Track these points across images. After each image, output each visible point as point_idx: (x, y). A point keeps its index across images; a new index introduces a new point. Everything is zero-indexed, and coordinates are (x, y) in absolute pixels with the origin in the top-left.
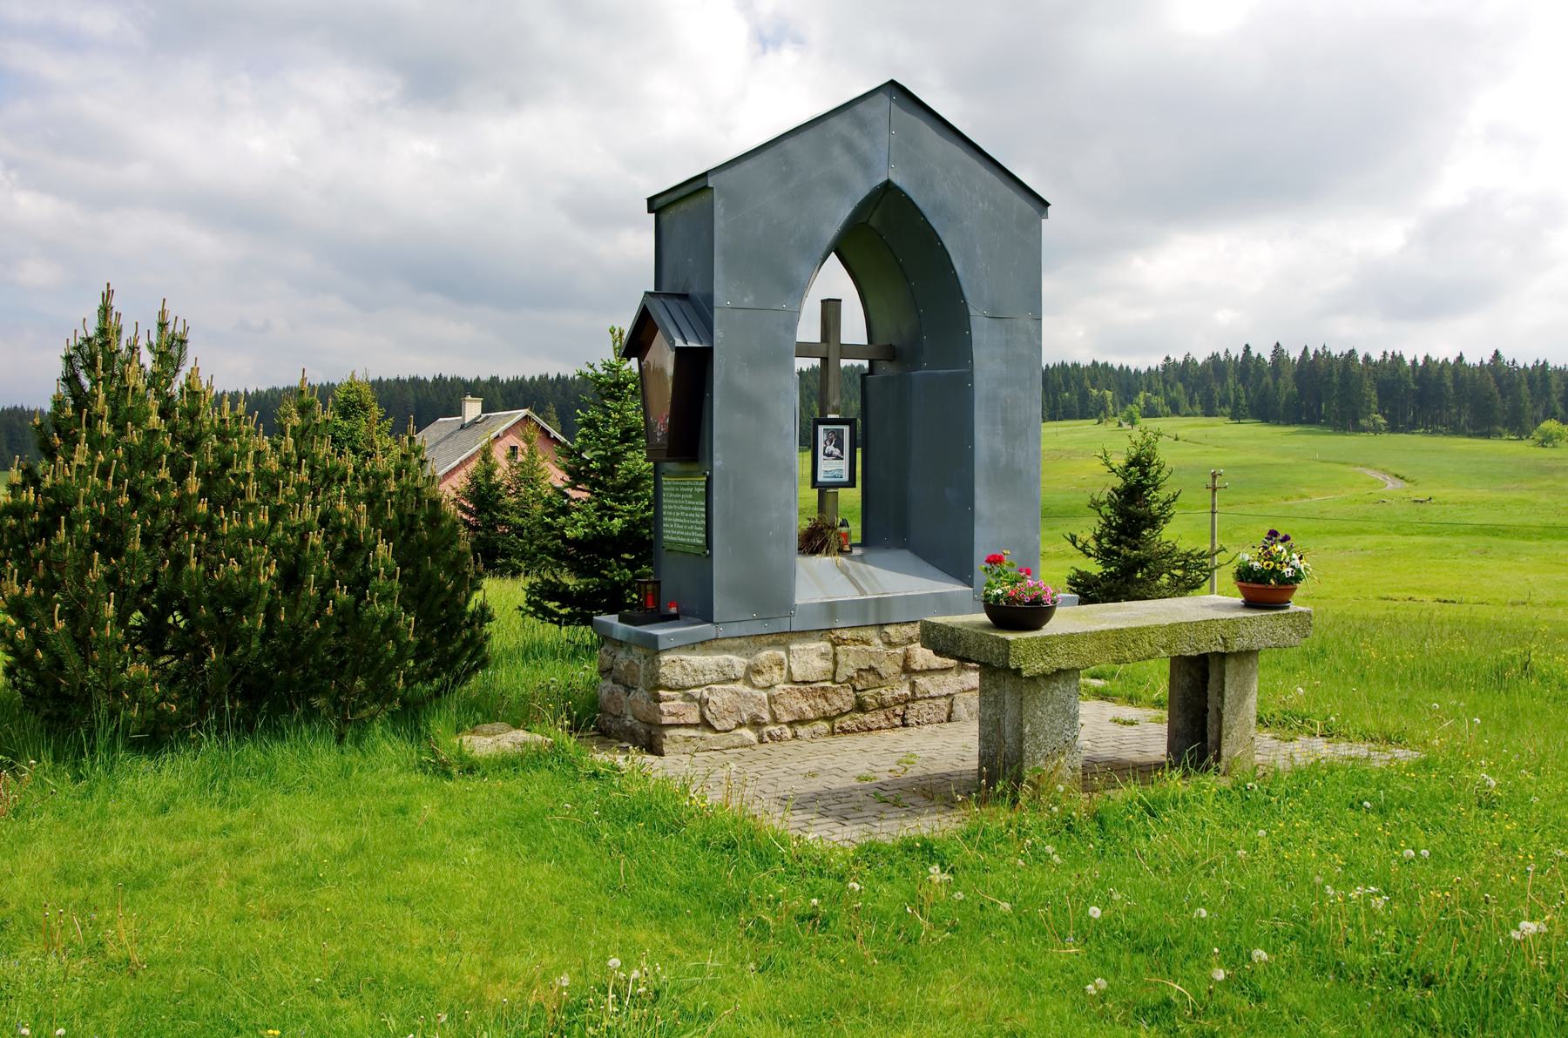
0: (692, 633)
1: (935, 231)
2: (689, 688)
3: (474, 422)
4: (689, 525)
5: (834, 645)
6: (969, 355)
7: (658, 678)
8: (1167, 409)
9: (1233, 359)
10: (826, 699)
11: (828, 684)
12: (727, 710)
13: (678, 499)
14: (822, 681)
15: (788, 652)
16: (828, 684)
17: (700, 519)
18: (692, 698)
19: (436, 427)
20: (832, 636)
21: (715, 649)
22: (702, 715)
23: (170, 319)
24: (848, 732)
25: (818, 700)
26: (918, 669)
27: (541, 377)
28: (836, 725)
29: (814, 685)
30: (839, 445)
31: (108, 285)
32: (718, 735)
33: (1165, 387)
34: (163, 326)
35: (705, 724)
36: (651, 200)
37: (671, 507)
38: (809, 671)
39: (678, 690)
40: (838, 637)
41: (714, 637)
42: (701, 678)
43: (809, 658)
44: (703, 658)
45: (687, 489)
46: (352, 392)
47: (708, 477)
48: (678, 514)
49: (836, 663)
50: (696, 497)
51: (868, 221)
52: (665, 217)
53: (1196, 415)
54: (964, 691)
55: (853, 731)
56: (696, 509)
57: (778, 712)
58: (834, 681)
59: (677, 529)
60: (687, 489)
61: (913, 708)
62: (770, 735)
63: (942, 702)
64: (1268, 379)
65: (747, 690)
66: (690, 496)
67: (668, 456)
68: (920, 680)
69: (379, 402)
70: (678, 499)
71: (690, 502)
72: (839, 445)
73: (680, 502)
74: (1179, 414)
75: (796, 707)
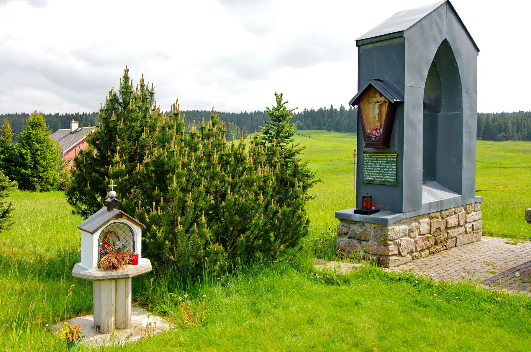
0: (398, 217)
1: (455, 59)
2: (395, 240)
3: (76, 131)
6: (461, 107)
8: (305, 127)
9: (327, 110)
11: (428, 235)
13: (375, 163)
15: (419, 223)
16: (428, 235)
19: (58, 133)
21: (401, 223)
22: (399, 251)
23: (145, 83)
27: (76, 114)
29: (425, 236)
31: (126, 66)
33: (305, 119)
34: (142, 86)
35: (400, 254)
36: (357, 41)
40: (431, 216)
41: (402, 218)
42: (399, 235)
43: (424, 225)
46: (35, 119)
49: (431, 226)
52: (360, 48)
53: (315, 129)
58: (430, 234)
63: (454, 239)
64: (339, 116)
65: (409, 239)
68: (450, 231)
69: (47, 122)
71: (385, 164)
73: (376, 164)
74: (309, 129)
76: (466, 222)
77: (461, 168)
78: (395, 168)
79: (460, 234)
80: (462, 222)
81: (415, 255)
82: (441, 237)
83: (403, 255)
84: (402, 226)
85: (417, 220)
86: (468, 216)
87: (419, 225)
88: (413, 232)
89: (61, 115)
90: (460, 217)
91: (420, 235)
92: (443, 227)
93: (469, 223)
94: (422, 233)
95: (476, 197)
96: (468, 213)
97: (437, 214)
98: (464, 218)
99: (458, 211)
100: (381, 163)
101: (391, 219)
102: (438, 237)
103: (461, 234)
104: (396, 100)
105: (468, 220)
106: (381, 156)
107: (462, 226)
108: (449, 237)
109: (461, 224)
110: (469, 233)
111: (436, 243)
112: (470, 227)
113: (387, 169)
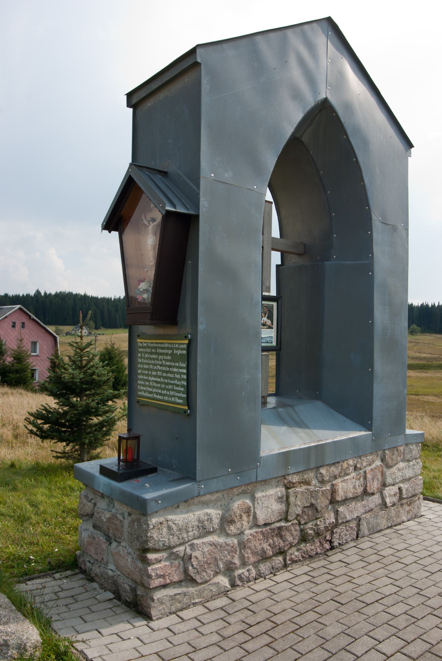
2: (174, 547)
4: (168, 384)
5: (287, 488)
7: (146, 542)
10: (281, 537)
11: (283, 524)
12: (206, 562)
13: (154, 359)
14: (278, 521)
15: (253, 499)
16: (283, 524)
17: (180, 380)
18: (177, 556)
20: (286, 482)
24: (296, 562)
25: (275, 539)
26: (340, 499)
27: (27, 294)
28: (288, 558)
29: (273, 526)
30: (270, 317)
32: (200, 587)
37: (146, 367)
38: (269, 515)
39: (165, 550)
40: (290, 482)
44: (186, 516)
45: (166, 351)
47: (190, 341)
48: (154, 373)
50: (175, 358)
51: (301, 136)
54: (366, 513)
55: (300, 561)
56: (175, 370)
57: (246, 555)
59: (154, 387)
60: (166, 351)
61: (336, 533)
62: (240, 578)
63: (353, 525)
66: (169, 358)
67: (151, 319)
68: (341, 509)
70: (154, 359)
71: (168, 363)
72: (270, 317)
73: (157, 362)
75: (259, 548)
76: (384, 485)
77: (371, 375)
78: (183, 373)
79: (369, 511)
80: (374, 486)
81: (240, 575)
82: (317, 525)
83: (199, 581)
84: (198, 513)
85: (247, 493)
86: (388, 472)
87: (254, 504)
88: (232, 522)
89: (11, 296)
90: (369, 476)
91: (256, 525)
92: (322, 502)
93: (393, 485)
94: (261, 522)
95: (408, 431)
96: (389, 467)
97: (306, 476)
98: (380, 477)
99: (365, 464)
100: (164, 360)
101: (156, 500)
102: (310, 525)
103: (372, 510)
104: (175, 206)
105: (389, 480)
106: (162, 343)
107: (373, 494)
108: (340, 521)
109: (369, 491)
110: (392, 506)
111: (304, 538)
112: (392, 493)
113: (172, 376)
